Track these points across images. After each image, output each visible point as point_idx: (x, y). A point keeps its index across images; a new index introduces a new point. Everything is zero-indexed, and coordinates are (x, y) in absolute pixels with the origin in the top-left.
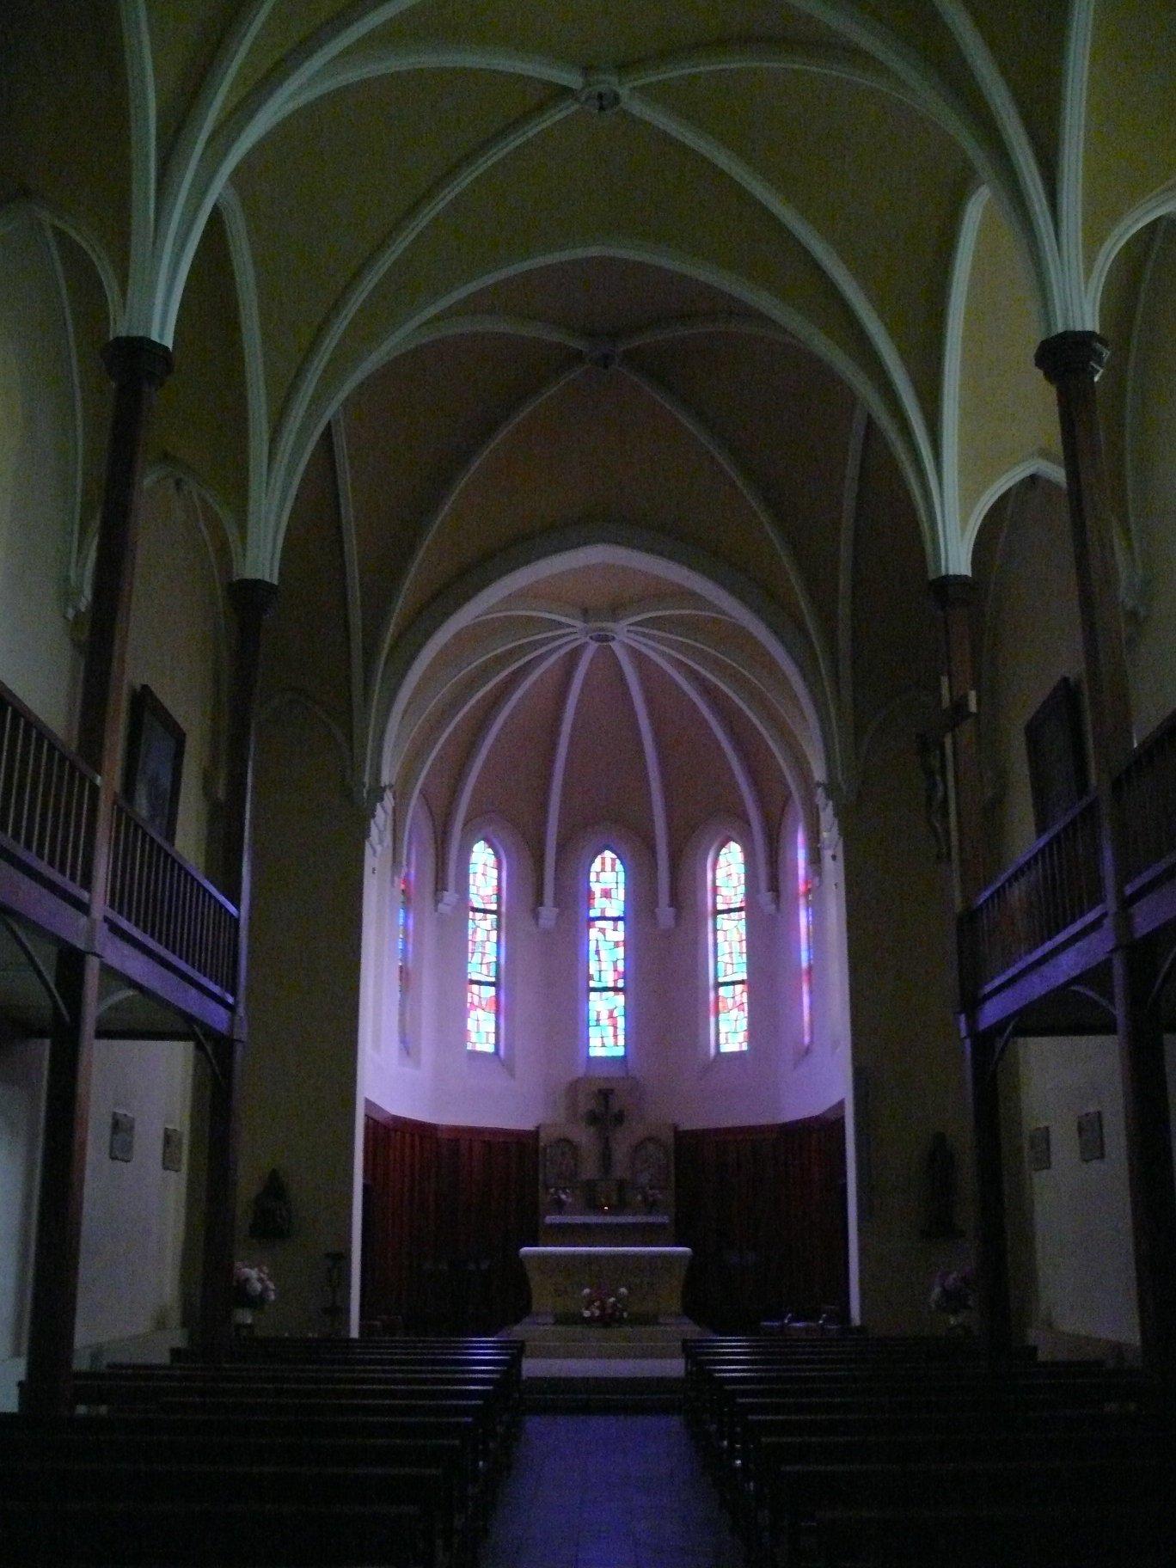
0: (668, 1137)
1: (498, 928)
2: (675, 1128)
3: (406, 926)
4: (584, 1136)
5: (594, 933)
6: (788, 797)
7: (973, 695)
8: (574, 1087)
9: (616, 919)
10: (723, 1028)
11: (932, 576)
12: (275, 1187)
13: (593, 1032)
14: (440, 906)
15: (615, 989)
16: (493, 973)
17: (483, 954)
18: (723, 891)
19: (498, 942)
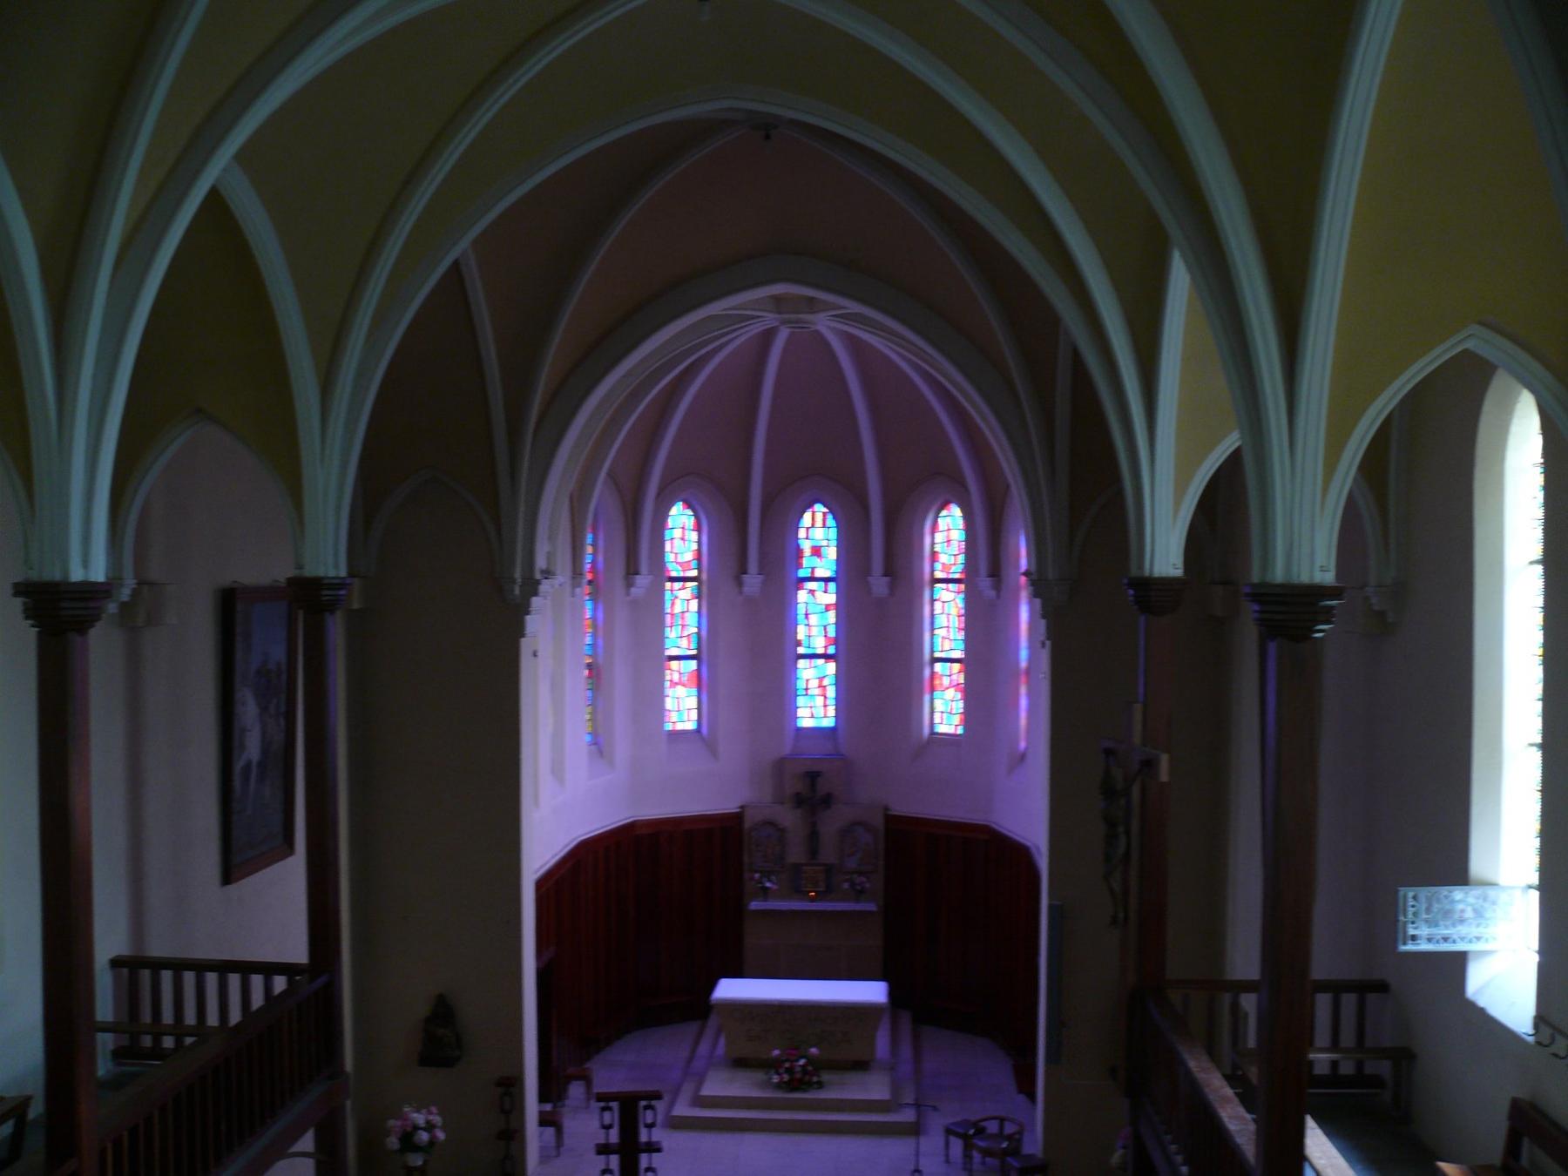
0: (878, 821)
1: (699, 597)
2: (886, 809)
3: (594, 618)
4: (789, 818)
5: (802, 596)
6: (1008, 486)
7: (1164, 759)
8: (780, 765)
9: (826, 580)
10: (939, 705)
11: (1134, 572)
12: (442, 1013)
13: (801, 701)
14: (633, 590)
15: (826, 657)
16: (694, 645)
17: (683, 626)
18: (943, 558)
19: (699, 612)
